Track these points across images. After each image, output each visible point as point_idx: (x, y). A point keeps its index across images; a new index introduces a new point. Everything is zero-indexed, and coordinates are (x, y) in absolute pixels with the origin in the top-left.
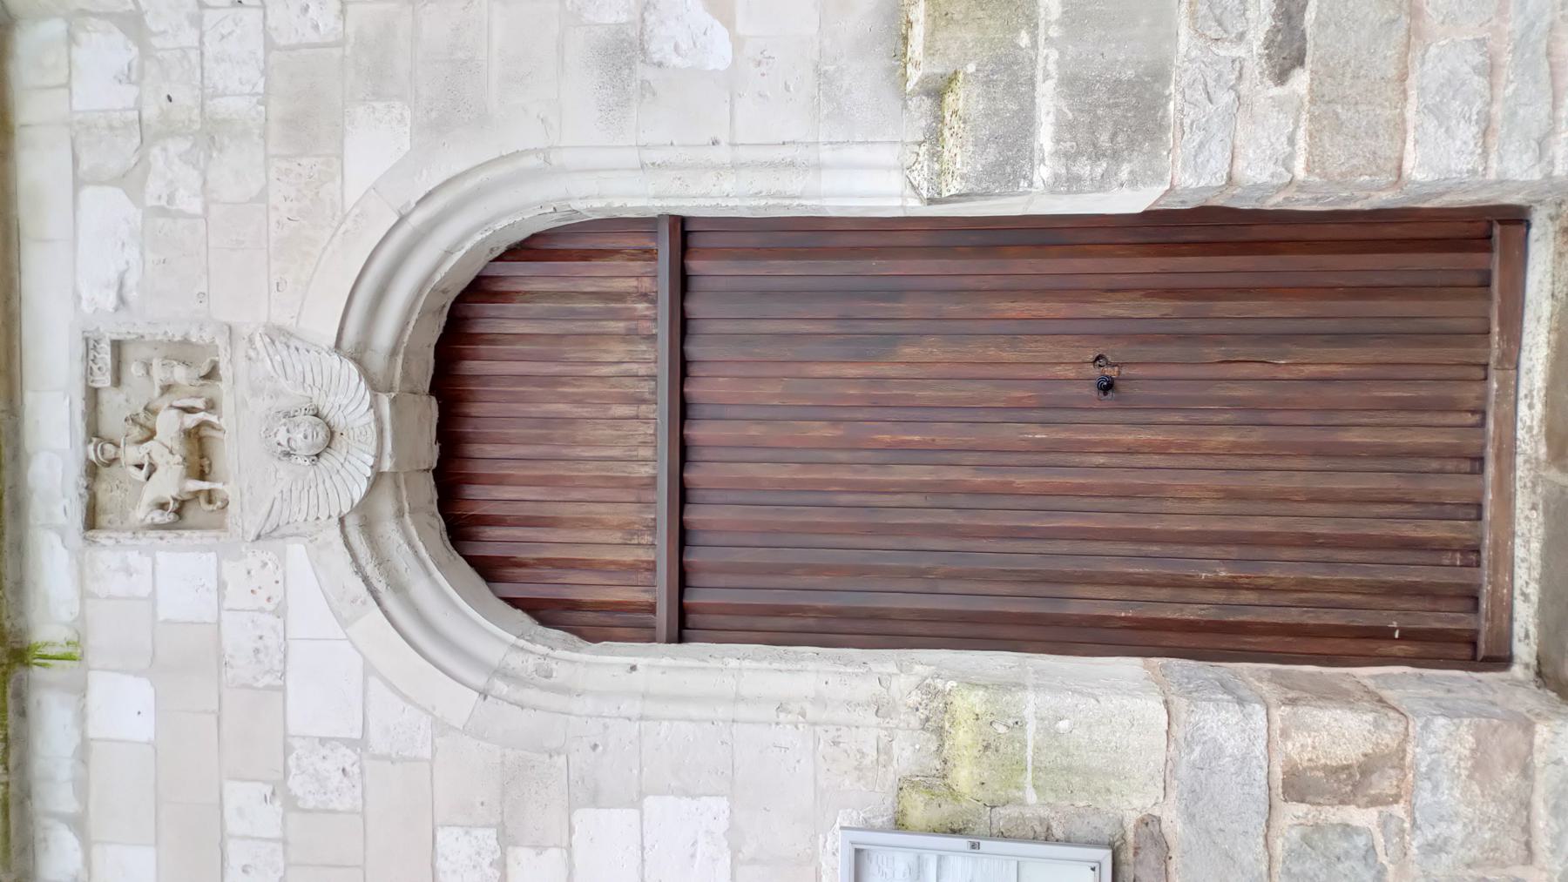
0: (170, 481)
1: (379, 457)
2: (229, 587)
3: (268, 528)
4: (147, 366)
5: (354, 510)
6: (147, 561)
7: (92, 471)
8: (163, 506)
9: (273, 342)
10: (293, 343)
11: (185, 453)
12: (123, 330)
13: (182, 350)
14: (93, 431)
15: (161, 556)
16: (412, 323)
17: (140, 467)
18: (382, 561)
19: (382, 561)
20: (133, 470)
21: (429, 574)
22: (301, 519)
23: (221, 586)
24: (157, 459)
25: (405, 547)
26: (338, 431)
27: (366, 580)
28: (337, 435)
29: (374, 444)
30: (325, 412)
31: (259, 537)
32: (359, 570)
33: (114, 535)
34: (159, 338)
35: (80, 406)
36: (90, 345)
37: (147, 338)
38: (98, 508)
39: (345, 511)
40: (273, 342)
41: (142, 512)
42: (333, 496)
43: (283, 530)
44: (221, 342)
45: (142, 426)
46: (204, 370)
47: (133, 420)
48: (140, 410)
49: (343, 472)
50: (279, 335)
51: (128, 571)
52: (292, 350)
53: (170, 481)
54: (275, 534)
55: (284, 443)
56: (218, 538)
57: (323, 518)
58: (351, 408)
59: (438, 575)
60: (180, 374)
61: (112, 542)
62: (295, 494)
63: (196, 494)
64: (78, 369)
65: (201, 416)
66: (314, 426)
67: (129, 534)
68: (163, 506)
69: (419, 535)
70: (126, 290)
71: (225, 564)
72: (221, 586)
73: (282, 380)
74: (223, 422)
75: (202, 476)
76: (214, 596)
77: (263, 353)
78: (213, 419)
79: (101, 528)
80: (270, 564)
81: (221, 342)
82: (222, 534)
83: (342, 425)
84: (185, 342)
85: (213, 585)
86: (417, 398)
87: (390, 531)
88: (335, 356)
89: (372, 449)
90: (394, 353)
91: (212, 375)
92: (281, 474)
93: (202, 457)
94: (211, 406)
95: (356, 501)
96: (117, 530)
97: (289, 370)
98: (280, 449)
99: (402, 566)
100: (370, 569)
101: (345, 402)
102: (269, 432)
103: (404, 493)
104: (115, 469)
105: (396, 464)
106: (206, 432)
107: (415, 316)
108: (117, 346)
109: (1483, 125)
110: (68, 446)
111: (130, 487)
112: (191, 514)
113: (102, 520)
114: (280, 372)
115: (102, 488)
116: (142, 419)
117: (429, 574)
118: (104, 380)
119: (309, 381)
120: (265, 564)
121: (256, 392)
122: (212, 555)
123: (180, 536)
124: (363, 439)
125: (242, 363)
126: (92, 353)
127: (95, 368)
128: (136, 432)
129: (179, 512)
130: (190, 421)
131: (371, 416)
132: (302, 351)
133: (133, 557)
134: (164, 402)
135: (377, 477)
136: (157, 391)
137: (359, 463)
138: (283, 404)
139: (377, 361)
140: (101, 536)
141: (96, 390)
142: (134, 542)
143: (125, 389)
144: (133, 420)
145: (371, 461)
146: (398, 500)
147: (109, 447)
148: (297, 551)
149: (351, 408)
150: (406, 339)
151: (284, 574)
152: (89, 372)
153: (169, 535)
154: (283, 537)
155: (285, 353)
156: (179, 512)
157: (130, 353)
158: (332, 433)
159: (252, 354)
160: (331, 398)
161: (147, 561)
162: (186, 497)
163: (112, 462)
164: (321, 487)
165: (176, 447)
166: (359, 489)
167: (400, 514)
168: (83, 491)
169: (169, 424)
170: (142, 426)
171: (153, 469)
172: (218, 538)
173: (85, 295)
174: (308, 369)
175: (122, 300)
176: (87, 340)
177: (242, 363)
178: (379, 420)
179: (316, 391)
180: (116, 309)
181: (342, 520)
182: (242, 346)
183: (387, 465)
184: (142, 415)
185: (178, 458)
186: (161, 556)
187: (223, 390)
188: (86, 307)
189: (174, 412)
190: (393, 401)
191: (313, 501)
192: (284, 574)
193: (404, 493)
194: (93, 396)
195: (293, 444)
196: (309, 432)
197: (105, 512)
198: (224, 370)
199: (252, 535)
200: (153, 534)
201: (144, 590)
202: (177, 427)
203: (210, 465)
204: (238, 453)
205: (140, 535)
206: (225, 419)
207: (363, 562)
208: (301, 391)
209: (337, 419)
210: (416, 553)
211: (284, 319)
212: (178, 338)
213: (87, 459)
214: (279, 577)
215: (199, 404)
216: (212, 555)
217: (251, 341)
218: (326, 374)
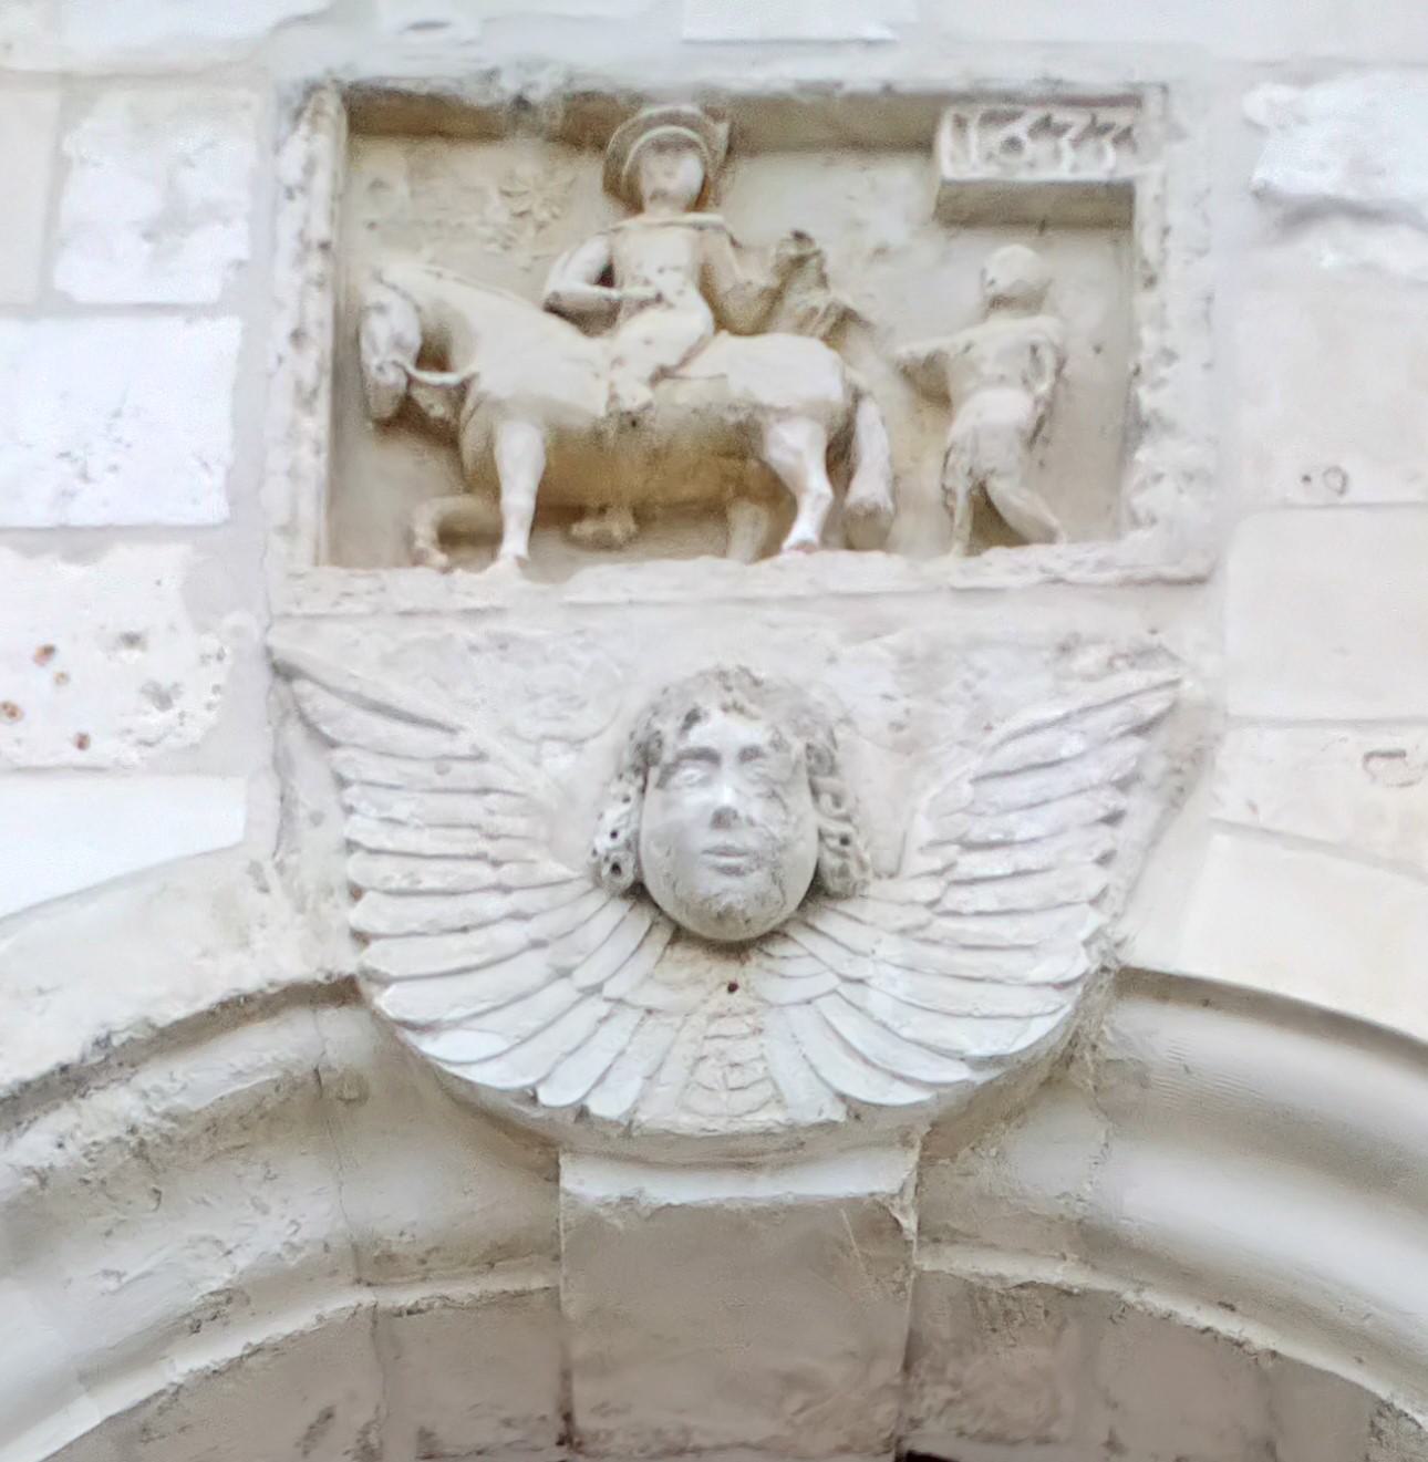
0: (533, 380)
1: (630, 1144)
2: (74, 572)
3: (321, 704)
4: (1024, 301)
5: (389, 1029)
6: (207, 288)
7: (588, 125)
8: (433, 355)
9: (1143, 729)
10: (1142, 809)
11: (661, 424)
12: (1177, 215)
13: (1093, 431)
14: (752, 131)
15: (226, 333)
16: (1228, 1325)
17: (606, 278)
18: (156, 1162)
19: (156, 1162)
20: (592, 255)
21: (92, 1375)
22: (363, 828)
23: (78, 542)
24: (633, 330)
25: (219, 1276)
26: (750, 972)
27: (67, 1083)
28: (730, 970)
29: (686, 1123)
30: (832, 922)
31: (284, 672)
32: (118, 1057)
33: (322, 182)
34: (1148, 335)
35: (862, 74)
36: (1111, 112)
37: (1145, 301)
38: (437, 147)
39: (388, 1001)
40: (1143, 729)
41: (403, 292)
42: (457, 951)
43: (311, 772)
44: (1139, 549)
45: (776, 296)
46: (1011, 495)
47: (800, 261)
48: (848, 299)
49: (562, 992)
50: (1172, 757)
51: (169, 226)
52: (1110, 800)
53: (533, 380)
54: (294, 733)
55: (698, 737)
56: (288, 530)
57: (358, 916)
58: (851, 1027)
59: (86, 1415)
60: (995, 409)
61: (293, 174)
62: (471, 808)
63: (484, 480)
64: (1015, 70)
65: (815, 488)
66: (771, 860)
67: (320, 229)
68: (433, 355)
69: (276, 1349)
70: (1344, 229)
71: (170, 559)
72: (78, 542)
73: (976, 764)
74: (787, 556)
75: (559, 512)
76: (38, 513)
77: (1089, 694)
78: (805, 526)
79: (352, 154)
80: (156, 719)
81: (1139, 549)
82: (305, 547)
83: (773, 989)
84: (1134, 427)
85: (86, 511)
86: (887, 1370)
87: (289, 1211)
88: (1080, 964)
89: (660, 1113)
90: (1097, 1240)
91: (990, 524)
92: (561, 762)
93: (643, 516)
94: (853, 530)
95: (430, 1047)
96: (339, 196)
97: (1024, 788)
98: (669, 727)
99: (131, 1257)
100: (118, 1106)
101: (878, 1002)
102: (742, 689)
103: (464, 1290)
104: (598, 205)
105: (592, 1226)
106: (747, 521)
107: (1260, 1337)
108: (1106, 212)
109: (247, 1071)
110: (690, 32)
111: (521, 257)
112: (404, 460)
113: (388, 160)
114: (1010, 755)
115: (522, 161)
116: (806, 297)
117: (92, 1375)
118: (965, 157)
119: (973, 864)
120: (163, 699)
121: (921, 667)
122: (213, 508)
123: (306, 401)
124: (707, 1073)
125: (1052, 619)
126: (1077, 120)
127: (1019, 129)
128: (749, 275)
129: (409, 415)
130: (796, 448)
131: (809, 1105)
132: (1105, 838)
133: (213, 252)
134: (872, 371)
135: (524, 1138)
136: (916, 346)
137: (597, 1058)
138: (869, 772)
139: (1055, 1164)
140: (322, 141)
141: (924, 145)
142: (288, 244)
143: (929, 247)
144: (800, 261)
145: (606, 1106)
146: (430, 1260)
147: (686, 173)
148: (221, 814)
149: (851, 1027)
150: (1158, 1301)
151: (119, 769)
152: (998, 107)
153: (311, 364)
154: (281, 765)
155: (1094, 772)
156: (409, 415)
157: (1076, 269)
158: (737, 950)
159: (1088, 659)
160: (891, 948)
161: (207, 288)
162: (470, 441)
163: (627, 195)
164: (494, 905)
165: (684, 395)
166: (476, 1054)
167: (372, 1261)
168: (509, 85)
169: (786, 377)
170: (776, 296)
171: (588, 320)
172: (288, 530)
173: (1323, 97)
174: (1027, 858)
175: (1302, 215)
176: (1131, 99)
177: (1052, 619)
178: (794, 1146)
179: (927, 890)
180: (1263, 195)
181: (344, 992)
182: (1128, 622)
183: (588, 1184)
184: (819, 299)
185: (635, 395)
186: (226, 333)
187: (912, 581)
188: (1262, 100)
189: (836, 394)
190: (875, 1220)
191: (431, 876)
192: (119, 769)
193: (464, 1290)
194: (894, 126)
195: (692, 771)
196: (746, 839)
197: (417, 173)
198: (998, 563)
199: (287, 644)
200: (319, 309)
201: (79, 275)
202: (766, 396)
203: (605, 545)
204: (660, 613)
205: (316, 264)
206: (805, 565)
207: (152, 1076)
208: (924, 830)
209: (799, 972)
210: (192, 1326)
211: (1243, 776)
212: (1147, 399)
213: (638, 100)
214: (101, 749)
215: (868, 486)
216: (213, 508)
217: (1141, 655)
218: (1005, 930)
